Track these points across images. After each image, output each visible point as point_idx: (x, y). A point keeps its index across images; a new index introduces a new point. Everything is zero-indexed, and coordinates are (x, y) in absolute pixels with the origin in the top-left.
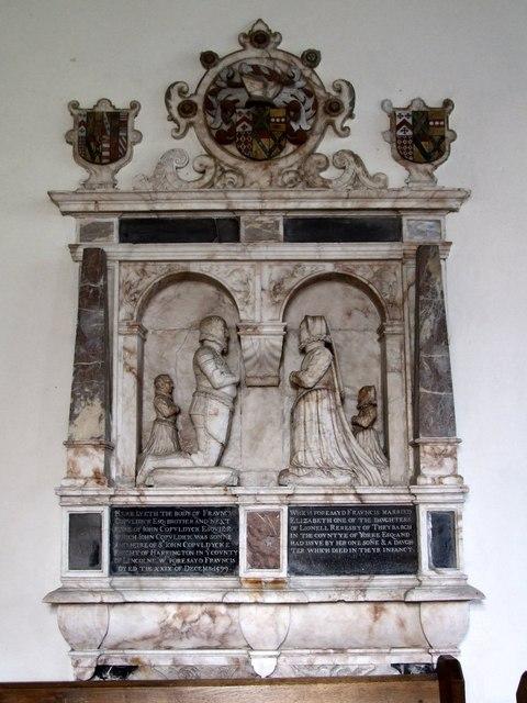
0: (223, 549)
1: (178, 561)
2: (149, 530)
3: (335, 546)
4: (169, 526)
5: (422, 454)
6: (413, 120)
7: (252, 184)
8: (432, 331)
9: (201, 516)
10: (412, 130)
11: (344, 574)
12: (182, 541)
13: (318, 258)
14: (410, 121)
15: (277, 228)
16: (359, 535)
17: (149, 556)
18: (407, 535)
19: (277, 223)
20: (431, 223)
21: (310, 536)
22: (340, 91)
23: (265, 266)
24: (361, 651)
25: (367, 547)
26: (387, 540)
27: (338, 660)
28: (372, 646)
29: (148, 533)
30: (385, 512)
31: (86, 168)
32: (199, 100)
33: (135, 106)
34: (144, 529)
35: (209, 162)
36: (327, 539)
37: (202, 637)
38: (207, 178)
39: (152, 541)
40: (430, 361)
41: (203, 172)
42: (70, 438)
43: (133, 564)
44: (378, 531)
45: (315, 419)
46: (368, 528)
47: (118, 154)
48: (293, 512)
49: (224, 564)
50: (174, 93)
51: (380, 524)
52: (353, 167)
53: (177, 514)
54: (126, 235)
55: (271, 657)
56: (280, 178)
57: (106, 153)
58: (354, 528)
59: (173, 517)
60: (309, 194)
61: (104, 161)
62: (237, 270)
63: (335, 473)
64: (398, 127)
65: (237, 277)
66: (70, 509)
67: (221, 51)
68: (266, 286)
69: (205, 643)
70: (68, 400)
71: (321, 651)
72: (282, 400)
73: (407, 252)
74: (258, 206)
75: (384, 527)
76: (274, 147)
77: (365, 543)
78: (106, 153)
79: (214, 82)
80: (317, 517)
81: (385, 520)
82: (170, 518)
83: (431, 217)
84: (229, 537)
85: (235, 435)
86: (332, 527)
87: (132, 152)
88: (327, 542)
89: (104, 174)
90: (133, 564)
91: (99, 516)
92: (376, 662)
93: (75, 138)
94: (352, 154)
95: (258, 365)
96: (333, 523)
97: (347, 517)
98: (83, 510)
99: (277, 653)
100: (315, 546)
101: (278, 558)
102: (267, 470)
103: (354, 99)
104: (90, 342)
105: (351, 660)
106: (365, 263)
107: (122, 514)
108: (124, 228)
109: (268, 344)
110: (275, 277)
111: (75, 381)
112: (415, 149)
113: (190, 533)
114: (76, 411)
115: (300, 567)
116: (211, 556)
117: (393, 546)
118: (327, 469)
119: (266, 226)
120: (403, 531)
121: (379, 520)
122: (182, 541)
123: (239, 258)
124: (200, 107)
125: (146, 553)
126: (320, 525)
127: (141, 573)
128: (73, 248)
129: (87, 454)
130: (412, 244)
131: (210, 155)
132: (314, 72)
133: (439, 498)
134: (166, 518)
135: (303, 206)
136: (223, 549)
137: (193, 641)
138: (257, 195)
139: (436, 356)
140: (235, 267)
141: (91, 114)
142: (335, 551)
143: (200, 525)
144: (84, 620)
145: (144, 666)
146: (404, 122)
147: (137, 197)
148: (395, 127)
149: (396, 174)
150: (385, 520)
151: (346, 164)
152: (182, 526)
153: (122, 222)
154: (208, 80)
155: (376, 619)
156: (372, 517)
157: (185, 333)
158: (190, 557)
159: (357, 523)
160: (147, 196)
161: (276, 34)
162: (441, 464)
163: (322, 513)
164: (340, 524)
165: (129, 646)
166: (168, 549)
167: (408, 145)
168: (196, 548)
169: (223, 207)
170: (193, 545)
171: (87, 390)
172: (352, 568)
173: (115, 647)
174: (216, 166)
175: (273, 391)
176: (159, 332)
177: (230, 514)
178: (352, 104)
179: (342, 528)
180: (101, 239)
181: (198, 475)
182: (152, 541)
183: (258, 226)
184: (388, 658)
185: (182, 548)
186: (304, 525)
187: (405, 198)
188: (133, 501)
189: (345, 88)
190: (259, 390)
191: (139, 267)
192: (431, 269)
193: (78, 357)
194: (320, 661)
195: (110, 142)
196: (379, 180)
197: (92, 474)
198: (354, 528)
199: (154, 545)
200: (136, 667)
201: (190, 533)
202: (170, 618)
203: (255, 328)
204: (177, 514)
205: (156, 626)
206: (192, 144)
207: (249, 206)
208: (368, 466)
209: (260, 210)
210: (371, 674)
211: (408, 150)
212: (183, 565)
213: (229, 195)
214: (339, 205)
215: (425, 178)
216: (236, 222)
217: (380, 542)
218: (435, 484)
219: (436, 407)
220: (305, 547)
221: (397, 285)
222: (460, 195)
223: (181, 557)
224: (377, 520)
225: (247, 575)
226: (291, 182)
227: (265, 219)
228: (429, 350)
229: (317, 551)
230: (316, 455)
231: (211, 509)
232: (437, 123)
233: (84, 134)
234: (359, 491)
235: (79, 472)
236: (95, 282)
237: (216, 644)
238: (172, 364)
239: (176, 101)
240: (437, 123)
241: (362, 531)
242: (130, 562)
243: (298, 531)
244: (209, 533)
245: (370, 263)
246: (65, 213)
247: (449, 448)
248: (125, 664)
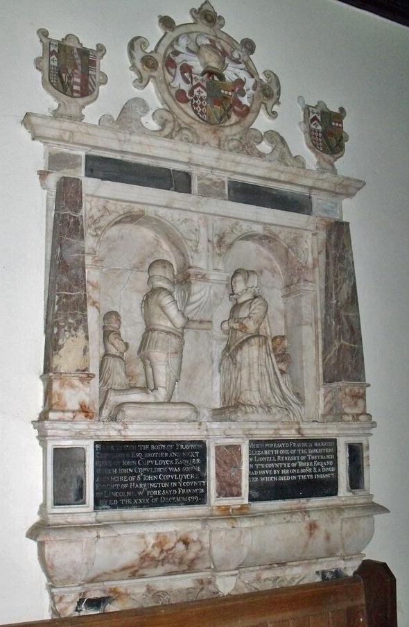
2: (128, 463)
3: (281, 475)
8: (348, 293)
9: (174, 450)
10: (321, 125)
17: (128, 489)
18: (331, 463)
25: (303, 474)
26: (318, 467)
27: (279, 572)
28: (304, 559)
30: (316, 444)
32: (159, 58)
33: (101, 49)
34: (124, 463)
35: (169, 117)
36: (275, 468)
37: (174, 563)
38: (167, 131)
39: (132, 474)
40: (347, 318)
46: (304, 458)
47: (87, 91)
51: (314, 454)
53: (153, 447)
54: (92, 171)
55: (232, 575)
61: (75, 94)
69: (175, 568)
77: (302, 471)
78: (76, 88)
80: (268, 449)
81: (316, 451)
86: (279, 457)
87: (98, 92)
88: (275, 472)
89: (73, 105)
96: (279, 454)
97: (289, 448)
98: (68, 443)
99: (237, 572)
100: (266, 475)
107: (107, 450)
116: (183, 487)
123: (193, 209)
125: (126, 486)
126: (270, 456)
128: (43, 175)
129: (72, 386)
131: (170, 111)
134: (143, 452)
135: (249, 171)
136: (193, 480)
137: (168, 567)
144: (67, 553)
146: (315, 118)
149: (311, 159)
154: (166, 42)
155: (311, 534)
157: (129, 272)
159: (296, 454)
161: (220, 18)
164: (285, 455)
165: (106, 577)
171: (70, 321)
173: (92, 581)
177: (200, 448)
178: (279, 93)
182: (132, 474)
183: (208, 183)
186: (258, 457)
191: (102, 202)
194: (266, 574)
197: (77, 407)
199: (133, 478)
202: (150, 547)
205: (137, 557)
206: (151, 93)
210: (301, 583)
221: (311, 247)
224: (311, 451)
225: (218, 504)
229: (268, 479)
230: (256, 394)
235: (65, 405)
237: (185, 567)
239: (139, 55)
241: (300, 460)
242: (107, 497)
244: (182, 466)
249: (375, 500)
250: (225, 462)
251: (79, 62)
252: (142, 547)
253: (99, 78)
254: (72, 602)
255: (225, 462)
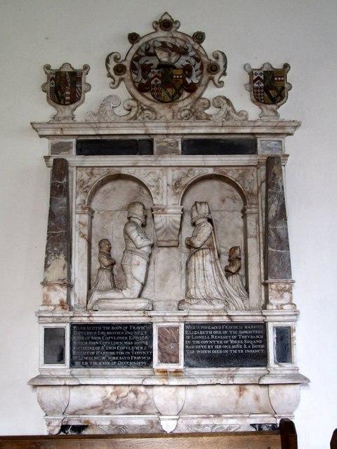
0: (142, 350)
1: (114, 358)
2: (95, 338)
3: (214, 349)
4: (108, 336)
5: (270, 290)
6: (264, 77)
7: (161, 117)
8: (276, 211)
9: (128, 330)
10: (264, 83)
11: (220, 366)
12: (116, 346)
13: (203, 165)
14: (262, 77)
15: (177, 146)
16: (230, 342)
17: (95, 355)
18: (261, 342)
19: (177, 142)
20: (276, 143)
21: (198, 342)
22: (217, 58)
23: (170, 170)
24: (231, 416)
25: (235, 349)
26: (248, 345)
27: (216, 421)
28: (238, 412)
29: (95, 341)
30: (246, 327)
31: (55, 107)
32: (127, 64)
33: (86, 67)
34: (92, 338)
35: (133, 103)
36: (209, 344)
37: (129, 407)
38: (132, 114)
39: (97, 345)
40: (275, 230)
41: (130, 110)
42: (45, 280)
43: (85, 361)
44: (241, 339)
45: (202, 268)
46: (235, 337)
47: (75, 98)
48: (188, 327)
49: (143, 360)
50: (111, 60)
51: (243, 335)
52: (225, 107)
53: (113, 328)
54: (81, 150)
55: (173, 419)
56: (179, 114)
57: (68, 98)
58: (226, 337)
59: (111, 330)
60: (197, 124)
61: (67, 103)
62: (152, 172)
63: (214, 302)
64: (255, 81)
65: (151, 177)
66: (45, 325)
67: (141, 33)
68: (170, 183)
69: (131, 411)
70: (44, 256)
71: (205, 416)
72: (180, 256)
73: (260, 161)
74: (165, 131)
75: (246, 337)
76: (175, 94)
77: (233, 347)
78: (68, 98)
79: (137, 53)
80: (203, 330)
81: (246, 332)
82: (108, 331)
83: (275, 139)
84: (147, 343)
85: (150, 278)
86: (212, 337)
87: (84, 97)
88: (209, 346)
89: (66, 111)
90: (85, 361)
91: (63, 329)
92: (240, 423)
93: (48, 88)
94: (225, 98)
95: (165, 233)
96: (213, 334)
97: (222, 330)
98: (53, 326)
99: (177, 417)
100: (201, 349)
101: (178, 356)
102: (171, 300)
103: (226, 63)
104: (58, 219)
105: (224, 422)
106: (234, 168)
107: (78, 328)
108: (79, 146)
109: (171, 220)
110: (176, 177)
111: (48, 243)
112: (266, 95)
113: (122, 341)
114: (48, 263)
115: (192, 362)
116: (135, 355)
117: (251, 349)
118: (209, 299)
119: (170, 144)
120: (258, 339)
121: (243, 332)
122: (116, 346)
123: (153, 165)
124: (128, 68)
125: (93, 353)
126: (205, 335)
127: (90, 366)
128: (47, 158)
129: (55, 290)
130: (263, 156)
131: (134, 99)
132: (201, 46)
133: (281, 318)
134: (106, 331)
135: (194, 131)
136: (142, 350)
137: (124, 410)
138: (164, 124)
139: (279, 227)
140: (150, 171)
141: (58, 73)
142: (214, 352)
143: (128, 336)
144: (54, 396)
145: (92, 425)
146: (258, 78)
147: (88, 126)
148: (252, 81)
149: (253, 111)
150: (246, 332)
151: (222, 105)
152: (116, 336)
153: (78, 142)
154: (133, 51)
155: (240, 395)
156: (238, 330)
157: (118, 213)
158: (122, 356)
159: (228, 334)
160: (94, 125)
161: (176, 22)
162: (282, 297)
163: (206, 328)
164: (218, 335)
165: (82, 412)
166: (107, 351)
167: (261, 93)
168: (125, 350)
169: (143, 132)
170: (123, 348)
171: (55, 249)
172: (225, 362)
173: (74, 413)
174: (138, 106)
175: (174, 249)
176: (102, 212)
178: (225, 66)
179: (219, 337)
180: (65, 153)
181: (126, 303)
182: (97, 345)
183: (165, 144)
184: (248, 420)
185: (116, 350)
186: (194, 336)
187: (259, 126)
188: (85, 320)
189: (221, 56)
190: (166, 249)
191: (89, 170)
192: (276, 172)
193: (50, 228)
194: (204, 422)
195: (70, 90)
196: (243, 115)
197: (59, 303)
198: (226, 337)
199: (98, 348)
200: (87, 426)
201: (122, 341)
202: (109, 394)
203: (163, 210)
204: (113, 328)
205: (100, 400)
206: (123, 92)
207: (159, 131)
208: (235, 298)
209: (167, 134)
210: (237, 431)
211: (261, 96)
212: (117, 361)
213: (146, 124)
214: (217, 131)
215: (272, 114)
216: (151, 142)
217: (243, 346)
218: (278, 309)
219: (279, 260)
220: (195, 349)
221: (254, 182)
222: (294, 124)
223: (116, 356)
224: (241, 332)
225: (158, 368)
226: (186, 116)
227: (170, 140)
228: (275, 224)
229: (202, 352)
230: (202, 291)
231: (135, 325)
232: (279, 79)
233: (54, 86)
234: (229, 314)
235: (51, 302)
236: (61, 180)
237: (138, 411)
238: (110, 233)
239: (113, 64)
240: (279, 79)
241: (232, 339)
242: (83, 359)
243: (190, 339)
244: (134, 341)
245: (237, 168)
246: (41, 136)
247: (287, 286)
248: (80, 424)
249: (300, 372)
250: (166, 339)
251: (69, 81)
252: (104, 394)
253: (84, 87)
254: (57, 426)
255: (166, 339)
